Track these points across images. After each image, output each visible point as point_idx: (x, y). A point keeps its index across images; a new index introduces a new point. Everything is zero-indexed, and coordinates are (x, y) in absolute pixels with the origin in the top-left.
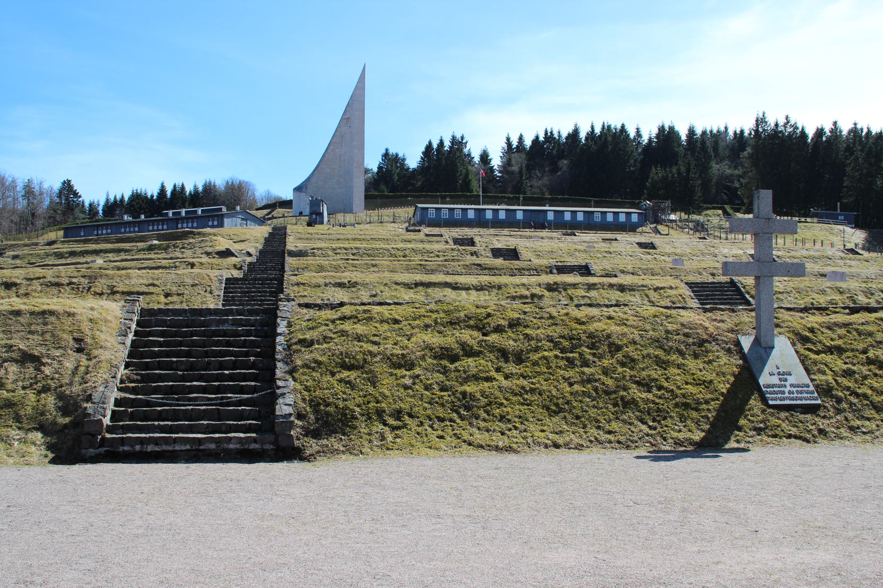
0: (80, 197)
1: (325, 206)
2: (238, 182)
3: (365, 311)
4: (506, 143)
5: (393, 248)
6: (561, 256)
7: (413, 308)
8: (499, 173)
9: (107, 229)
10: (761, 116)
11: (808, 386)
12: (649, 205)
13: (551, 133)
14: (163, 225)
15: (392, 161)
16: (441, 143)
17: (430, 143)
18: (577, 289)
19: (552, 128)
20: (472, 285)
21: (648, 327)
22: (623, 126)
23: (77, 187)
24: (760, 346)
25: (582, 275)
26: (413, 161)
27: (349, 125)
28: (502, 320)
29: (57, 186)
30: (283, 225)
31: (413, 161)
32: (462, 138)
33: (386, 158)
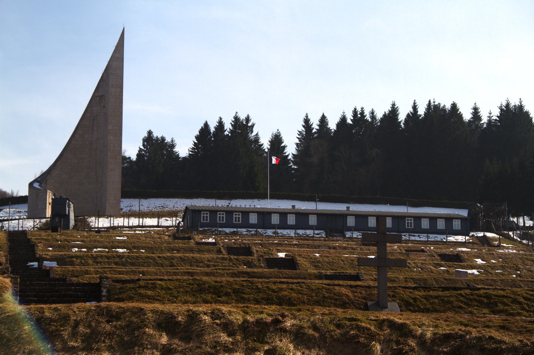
1: (72, 206)
3: (152, 284)
4: (304, 126)
6: (342, 268)
7: (179, 282)
8: (294, 165)
12: (480, 207)
13: (362, 113)
16: (221, 125)
17: (206, 125)
19: (362, 108)
21: (314, 294)
22: (454, 106)
28: (229, 290)
30: (17, 229)
32: (248, 119)
33: (148, 144)
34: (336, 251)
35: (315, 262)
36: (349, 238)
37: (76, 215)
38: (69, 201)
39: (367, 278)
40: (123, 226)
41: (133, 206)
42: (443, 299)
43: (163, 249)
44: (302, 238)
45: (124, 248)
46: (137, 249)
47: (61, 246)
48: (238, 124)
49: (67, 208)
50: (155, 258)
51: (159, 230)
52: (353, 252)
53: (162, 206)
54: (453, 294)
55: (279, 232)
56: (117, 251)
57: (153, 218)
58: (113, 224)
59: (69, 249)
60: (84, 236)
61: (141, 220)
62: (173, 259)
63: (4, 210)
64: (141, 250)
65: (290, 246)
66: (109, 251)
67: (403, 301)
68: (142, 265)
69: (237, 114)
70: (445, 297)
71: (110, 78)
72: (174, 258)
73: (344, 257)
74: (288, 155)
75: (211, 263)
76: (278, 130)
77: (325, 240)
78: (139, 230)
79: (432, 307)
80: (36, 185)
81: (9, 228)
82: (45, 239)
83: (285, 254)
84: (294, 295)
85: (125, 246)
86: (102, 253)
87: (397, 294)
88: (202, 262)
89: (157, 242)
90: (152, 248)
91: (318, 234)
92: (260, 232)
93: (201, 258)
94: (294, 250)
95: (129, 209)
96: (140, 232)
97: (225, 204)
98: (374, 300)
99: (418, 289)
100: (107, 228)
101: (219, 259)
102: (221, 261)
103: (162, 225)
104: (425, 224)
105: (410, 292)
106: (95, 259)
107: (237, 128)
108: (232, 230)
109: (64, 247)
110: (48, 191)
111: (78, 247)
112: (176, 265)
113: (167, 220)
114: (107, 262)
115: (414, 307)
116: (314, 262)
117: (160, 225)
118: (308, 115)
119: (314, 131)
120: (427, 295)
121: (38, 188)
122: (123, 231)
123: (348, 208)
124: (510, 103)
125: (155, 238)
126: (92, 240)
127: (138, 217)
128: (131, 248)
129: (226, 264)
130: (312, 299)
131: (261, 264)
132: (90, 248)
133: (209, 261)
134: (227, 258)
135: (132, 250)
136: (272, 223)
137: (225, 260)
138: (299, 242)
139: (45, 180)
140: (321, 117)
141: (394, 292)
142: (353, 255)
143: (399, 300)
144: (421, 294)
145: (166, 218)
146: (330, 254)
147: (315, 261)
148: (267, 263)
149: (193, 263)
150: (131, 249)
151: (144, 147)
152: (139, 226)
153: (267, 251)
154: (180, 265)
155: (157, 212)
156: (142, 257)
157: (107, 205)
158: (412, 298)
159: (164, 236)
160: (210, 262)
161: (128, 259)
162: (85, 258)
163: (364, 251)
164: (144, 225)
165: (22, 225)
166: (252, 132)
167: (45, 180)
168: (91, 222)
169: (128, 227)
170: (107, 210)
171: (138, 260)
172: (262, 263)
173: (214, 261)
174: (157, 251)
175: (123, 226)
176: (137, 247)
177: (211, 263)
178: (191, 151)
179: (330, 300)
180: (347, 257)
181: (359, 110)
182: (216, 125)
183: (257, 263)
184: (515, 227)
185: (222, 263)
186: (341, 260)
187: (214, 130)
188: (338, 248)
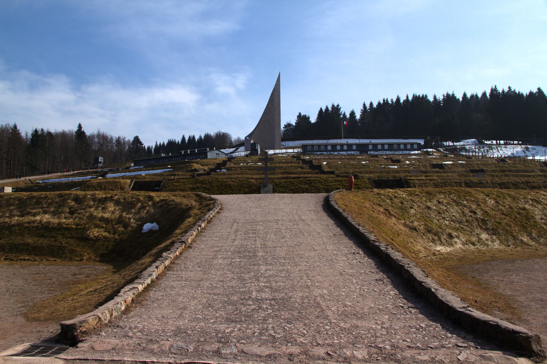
0: (143, 144)
1: (259, 146)
2: (222, 134)
9: (153, 161)
10: (494, 87)
13: (387, 100)
14: (179, 158)
15: (303, 119)
16: (327, 108)
17: (321, 109)
19: (387, 98)
23: (142, 139)
25: (471, 181)
26: (313, 119)
29: (132, 139)
31: (313, 119)
32: (338, 106)
33: (299, 118)
84: (232, 183)
95: (287, 145)
100: (273, 154)
104: (402, 147)
108: (320, 153)
119: (367, 109)
123: (370, 141)
124: (174, 140)
133: (286, 167)
152: (286, 153)
169: (281, 153)
180: (352, 163)
181: (386, 99)
184: (443, 146)
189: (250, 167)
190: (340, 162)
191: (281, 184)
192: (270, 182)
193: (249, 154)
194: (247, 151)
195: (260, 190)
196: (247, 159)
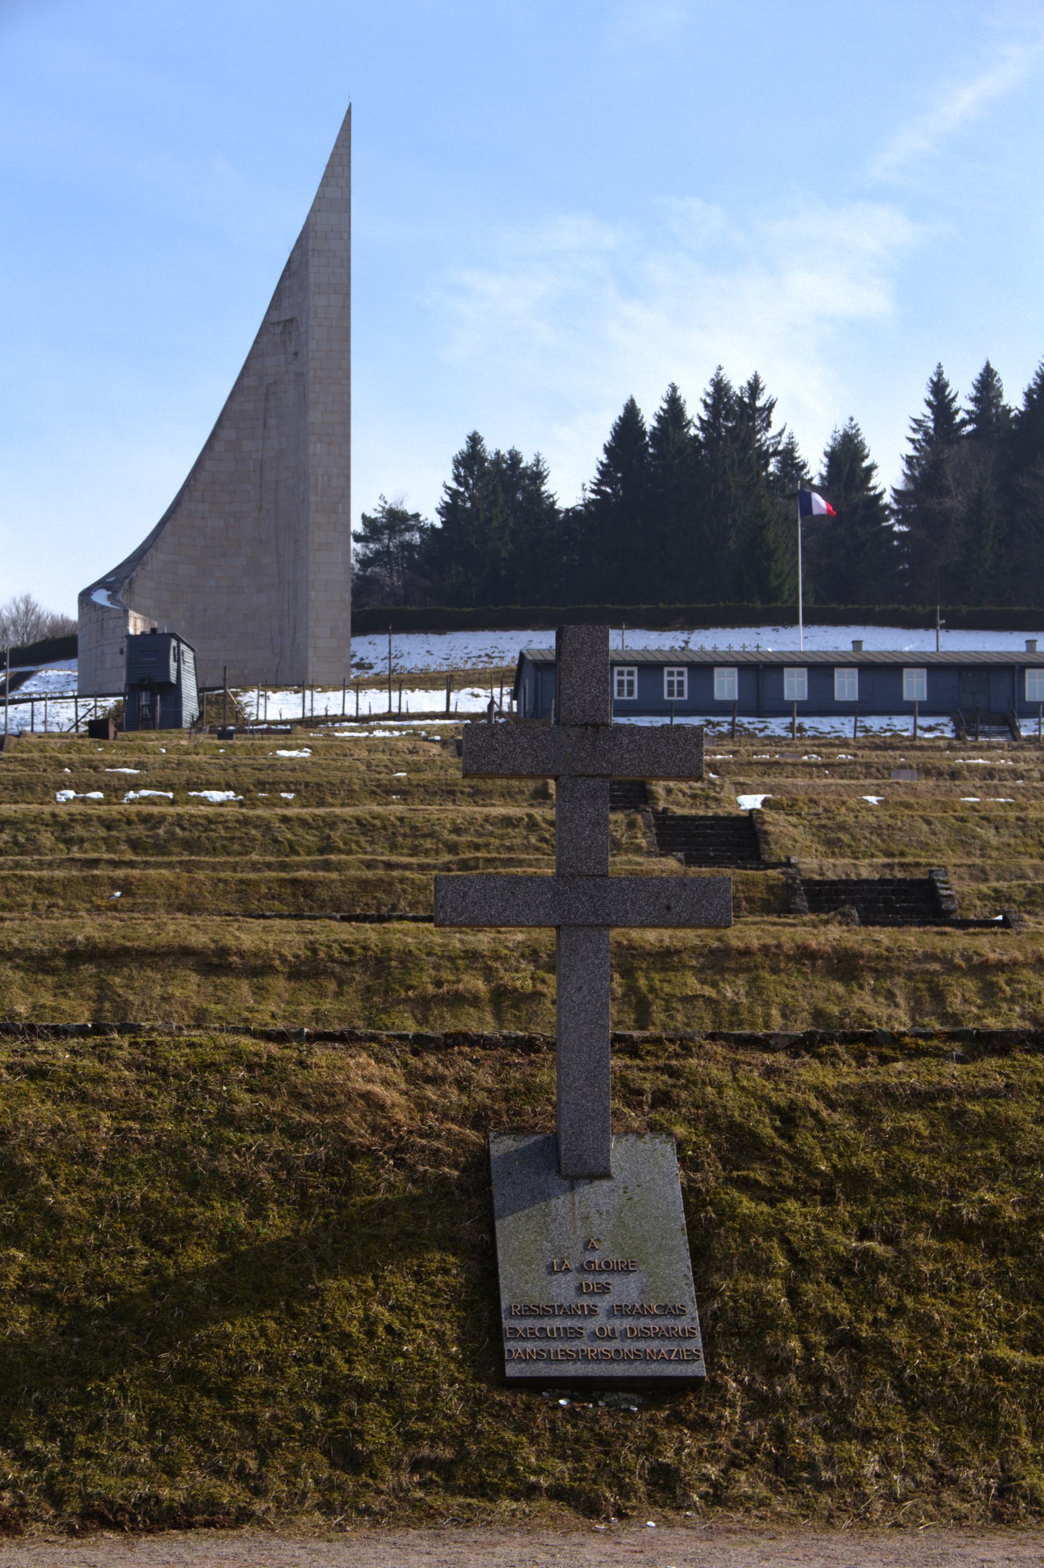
1: (188, 656)
4: (929, 404)
5: (285, 819)
6: (924, 846)
8: (900, 522)
11: (680, 1312)
16: (674, 406)
17: (631, 412)
18: (674, 969)
20: (283, 959)
24: (559, 1172)
27: (291, 349)
32: (754, 388)
34: (938, 786)
35: (830, 828)
36: (1029, 739)
37: (201, 686)
38: (179, 640)
39: (966, 889)
40: (343, 714)
41: (402, 656)
42: (962, 1112)
43: (357, 788)
44: (877, 741)
45: (228, 787)
46: (270, 791)
47: (20, 784)
48: (725, 404)
49: (173, 665)
50: (269, 822)
51: (445, 726)
52: (996, 787)
53: (487, 655)
54: (1027, 1076)
55: (806, 726)
56: (205, 797)
57: (434, 689)
58: (312, 710)
59: (47, 794)
60: (179, 749)
61: (395, 695)
62: (333, 826)
63: (39, 674)
64: (284, 795)
65: (807, 770)
66: (178, 798)
67: (717, 1129)
68: (224, 847)
69: (722, 373)
70: (973, 1097)
71: (311, 264)
72: (335, 823)
73: (964, 805)
74: (881, 494)
75: (465, 839)
76: (852, 419)
77: (951, 748)
78: (385, 728)
79: (889, 1166)
80: (101, 597)
81: (9, 727)
82: (23, 760)
83: (761, 797)
85: (232, 781)
86: (154, 804)
87: (685, 1087)
88: (431, 835)
89: (377, 766)
90: (319, 785)
91: (930, 729)
92: (747, 726)
93: (429, 821)
94: (793, 785)
96: (387, 734)
97: (673, 643)
98: (531, 1130)
99: (824, 1049)
101: (492, 825)
102: (500, 832)
103: (459, 710)
105: (770, 1072)
106: (63, 830)
107: (720, 415)
109: (30, 787)
110: (131, 613)
111: (77, 785)
112: (341, 845)
113: (477, 696)
114: (103, 839)
115: (778, 1164)
116: (824, 826)
117: (452, 709)
118: (943, 369)
119: (958, 419)
120: (868, 1086)
121: (103, 607)
122: (336, 731)
123: (1031, 643)
125: (398, 752)
126: (169, 763)
127: (398, 686)
128: (252, 787)
129: (515, 841)
130: (142, 1131)
131: (636, 838)
132: (116, 790)
133: (457, 830)
134: (523, 819)
135: (253, 794)
136: (786, 698)
137: (515, 826)
138: (855, 755)
139: (127, 580)
140: (981, 375)
141: (672, 1072)
142: (994, 797)
143: (690, 1122)
144: (831, 1081)
145: (473, 688)
146: (916, 796)
147: (830, 823)
148: (657, 835)
149: (400, 839)
150: (250, 791)
151: (459, 484)
152: (389, 716)
153: (703, 790)
154: (354, 846)
155: (463, 671)
156: (226, 821)
157: (311, 651)
158: (775, 1110)
159: (426, 743)
160: (459, 835)
161: (178, 830)
162: (31, 827)
163: (1035, 784)
164: (404, 710)
165: (42, 718)
166: (769, 424)
167: (127, 580)
168: (247, 705)
169: (356, 719)
170: (310, 669)
171: (212, 830)
172: (639, 835)
173: (476, 831)
174: (334, 795)
175: (343, 714)
176: (269, 783)
177: (465, 839)
178: (593, 491)
179: (260, 1138)
182: (661, 408)
183: (622, 835)
185: (501, 837)
186: (921, 817)
187: (655, 424)
188: (965, 773)
189: (146, 819)
190: (873, 799)
191: (806, 1139)
192: (632, 1095)
193: (116, 713)
194: (96, 695)
195: (488, 1224)
196: (98, 751)
